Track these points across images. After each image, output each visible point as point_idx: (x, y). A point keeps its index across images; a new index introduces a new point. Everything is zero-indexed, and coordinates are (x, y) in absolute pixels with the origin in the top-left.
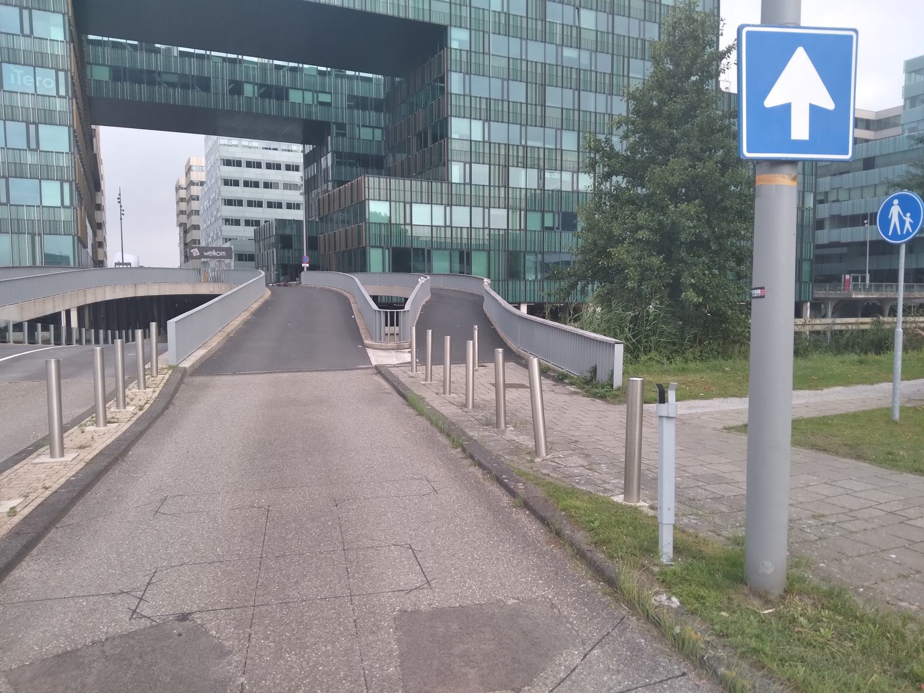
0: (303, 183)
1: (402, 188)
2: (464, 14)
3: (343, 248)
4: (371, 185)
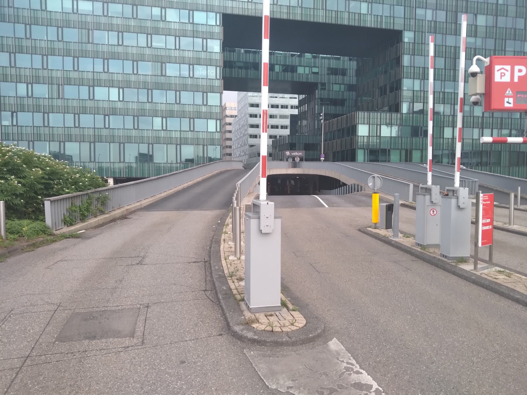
1: (376, 117)
2: (411, 24)
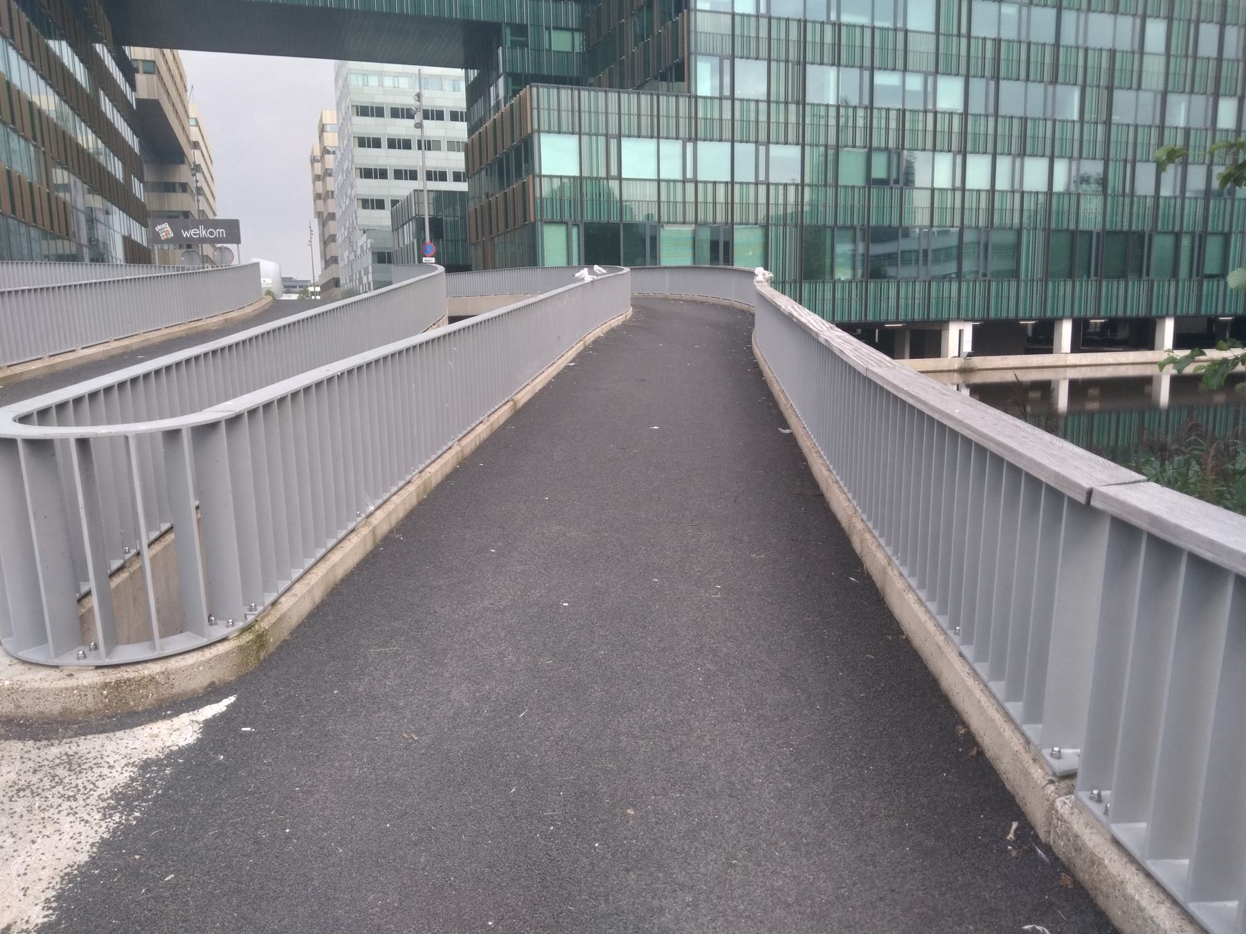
1: (602, 108)
4: (544, 104)
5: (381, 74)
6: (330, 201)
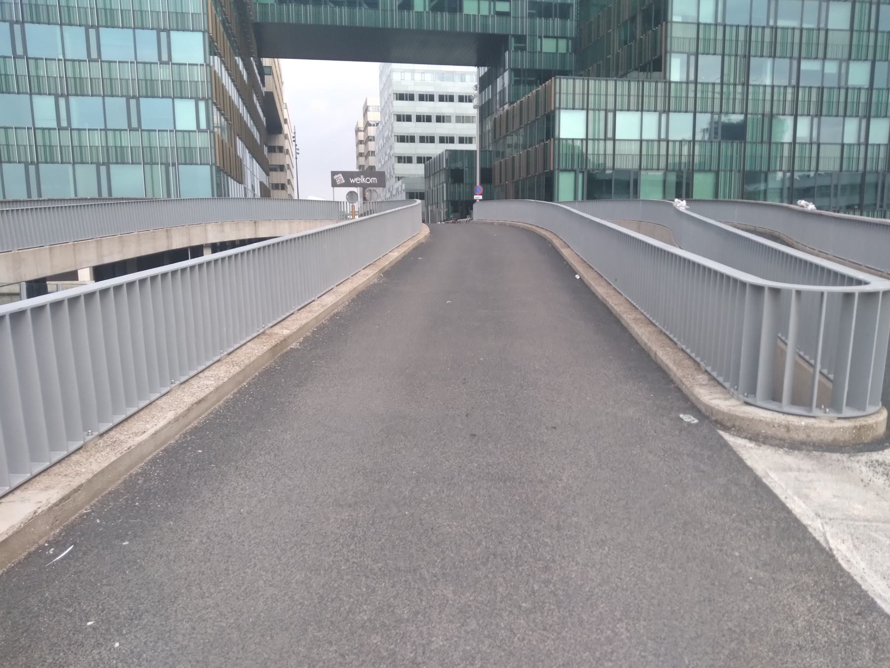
0: (476, 92)
1: (603, 92)
3: (523, 175)
5: (413, 72)
6: (371, 158)
